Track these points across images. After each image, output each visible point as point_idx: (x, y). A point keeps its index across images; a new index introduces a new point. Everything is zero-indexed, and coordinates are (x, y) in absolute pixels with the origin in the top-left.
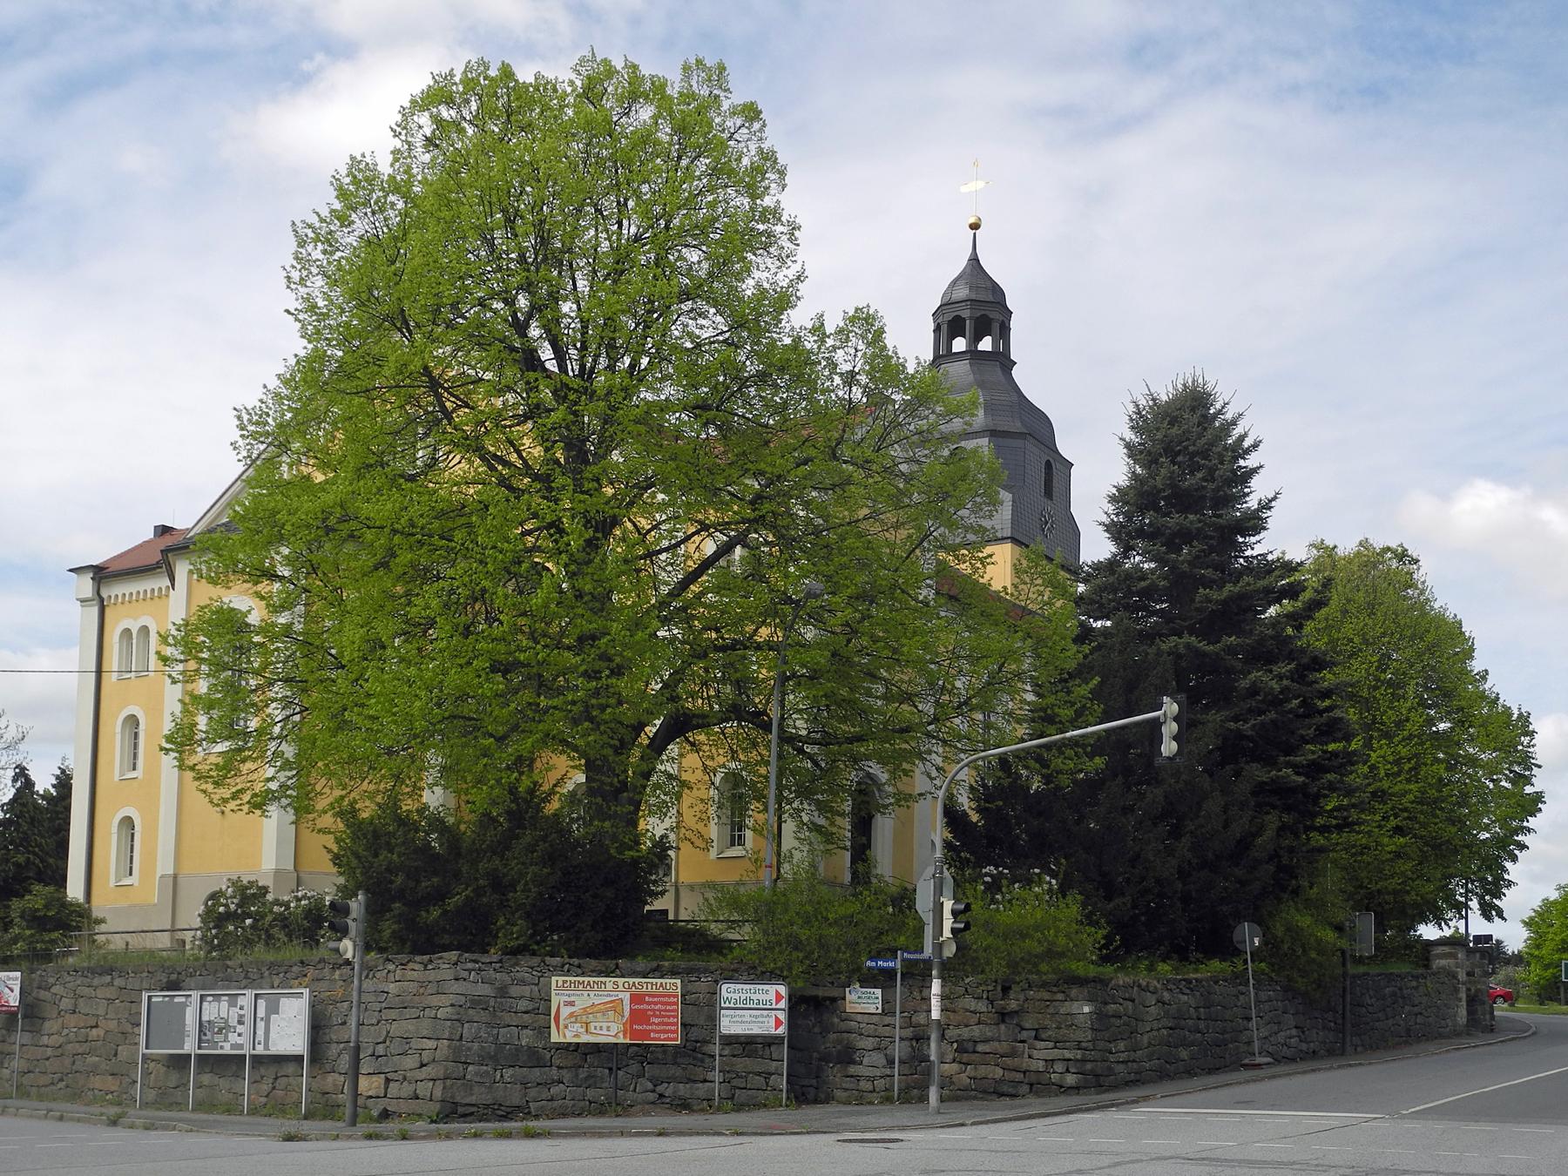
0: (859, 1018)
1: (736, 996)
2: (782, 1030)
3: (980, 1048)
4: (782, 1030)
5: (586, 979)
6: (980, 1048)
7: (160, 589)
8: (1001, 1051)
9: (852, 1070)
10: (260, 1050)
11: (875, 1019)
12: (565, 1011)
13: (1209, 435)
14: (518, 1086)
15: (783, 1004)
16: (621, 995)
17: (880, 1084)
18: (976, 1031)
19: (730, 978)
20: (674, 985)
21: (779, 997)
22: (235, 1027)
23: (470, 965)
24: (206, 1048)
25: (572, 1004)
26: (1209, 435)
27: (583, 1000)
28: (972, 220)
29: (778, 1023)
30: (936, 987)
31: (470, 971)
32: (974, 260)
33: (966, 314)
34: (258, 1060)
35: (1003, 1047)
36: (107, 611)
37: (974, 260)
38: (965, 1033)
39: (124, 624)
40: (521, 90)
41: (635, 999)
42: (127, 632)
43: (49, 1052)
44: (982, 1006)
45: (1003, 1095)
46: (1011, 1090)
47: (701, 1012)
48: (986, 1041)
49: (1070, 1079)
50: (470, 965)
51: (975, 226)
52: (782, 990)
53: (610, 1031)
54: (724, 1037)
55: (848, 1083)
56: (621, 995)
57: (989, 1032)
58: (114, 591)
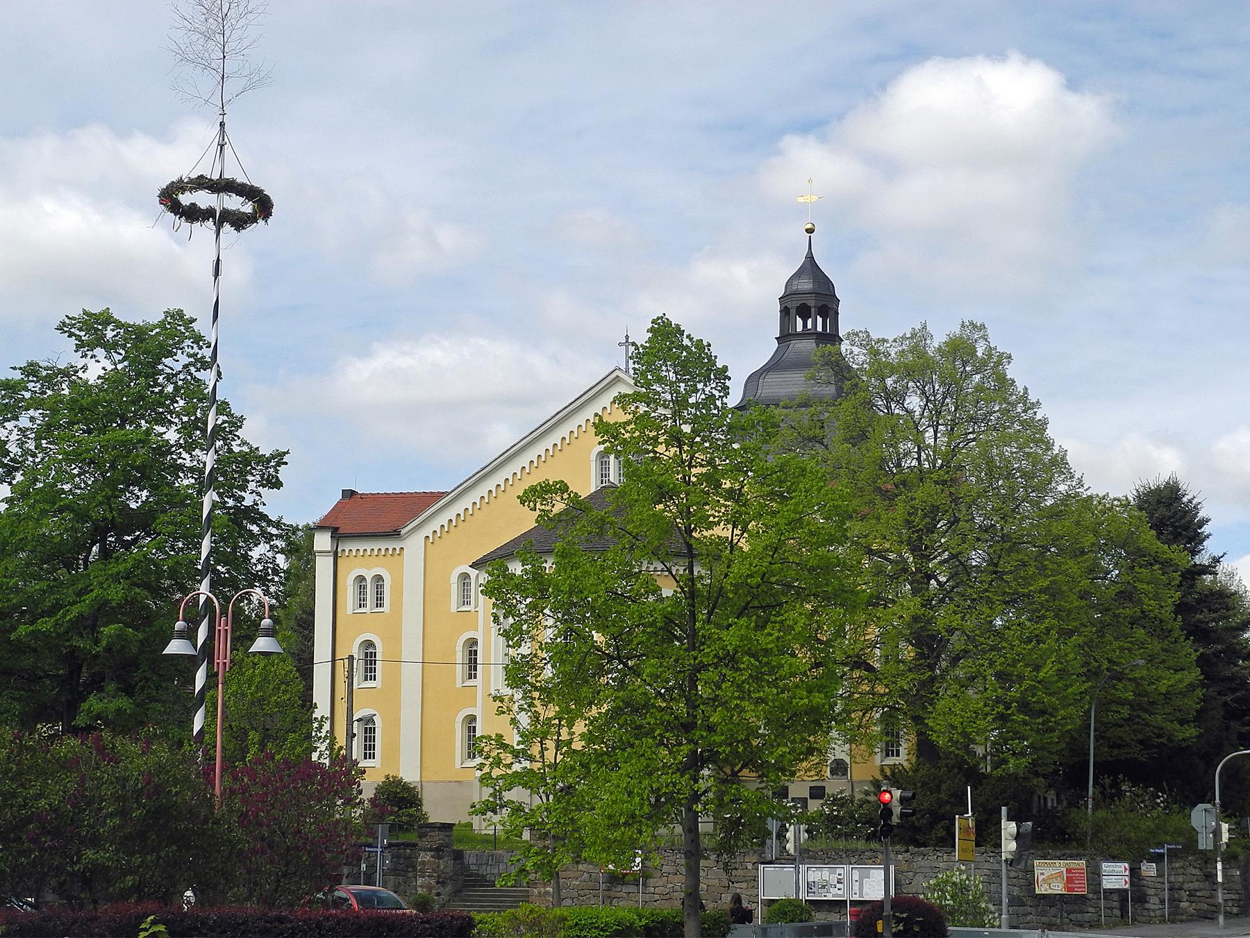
0: (1147, 879)
1: (1108, 869)
2: (1127, 886)
3: (1198, 894)
4: (1127, 886)
5: (1048, 861)
6: (1198, 894)
7: (394, 549)
8: (1207, 895)
9: (1147, 906)
10: (856, 898)
11: (1153, 879)
12: (1041, 878)
13: (1188, 519)
14: (1015, 916)
15: (1127, 873)
16: (1062, 869)
17: (1158, 913)
18: (1196, 885)
19: (1107, 860)
20: (1082, 863)
21: (1126, 869)
22: (835, 885)
23: (991, 854)
24: (811, 896)
25: (1043, 874)
26: (1188, 519)
27: (1049, 872)
28: (809, 226)
29: (1126, 882)
30: (1219, 866)
31: (990, 857)
32: (810, 258)
33: (811, 303)
34: (853, 903)
35: (1207, 893)
36: (339, 559)
37: (810, 258)
38: (1191, 886)
39: (359, 572)
40: (1004, 383)
41: (1068, 871)
42: (361, 579)
43: (657, 897)
44: (1197, 872)
45: (1207, 918)
46: (1211, 916)
47: (1095, 876)
48: (1199, 890)
49: (1235, 910)
50: (991, 854)
51: (810, 231)
52: (1127, 865)
53: (1058, 888)
54: (1104, 889)
55: (1145, 913)
56: (1062, 869)
57: (1202, 885)
58: (348, 546)
